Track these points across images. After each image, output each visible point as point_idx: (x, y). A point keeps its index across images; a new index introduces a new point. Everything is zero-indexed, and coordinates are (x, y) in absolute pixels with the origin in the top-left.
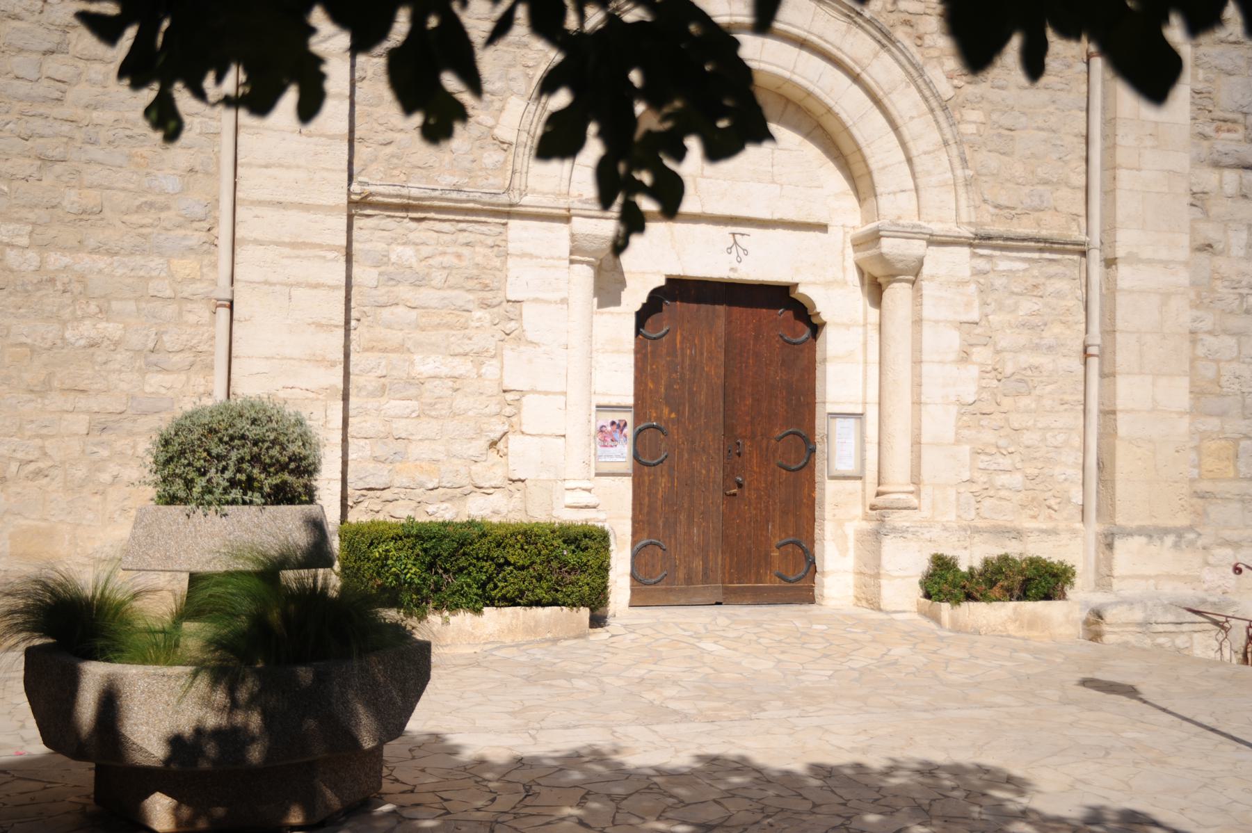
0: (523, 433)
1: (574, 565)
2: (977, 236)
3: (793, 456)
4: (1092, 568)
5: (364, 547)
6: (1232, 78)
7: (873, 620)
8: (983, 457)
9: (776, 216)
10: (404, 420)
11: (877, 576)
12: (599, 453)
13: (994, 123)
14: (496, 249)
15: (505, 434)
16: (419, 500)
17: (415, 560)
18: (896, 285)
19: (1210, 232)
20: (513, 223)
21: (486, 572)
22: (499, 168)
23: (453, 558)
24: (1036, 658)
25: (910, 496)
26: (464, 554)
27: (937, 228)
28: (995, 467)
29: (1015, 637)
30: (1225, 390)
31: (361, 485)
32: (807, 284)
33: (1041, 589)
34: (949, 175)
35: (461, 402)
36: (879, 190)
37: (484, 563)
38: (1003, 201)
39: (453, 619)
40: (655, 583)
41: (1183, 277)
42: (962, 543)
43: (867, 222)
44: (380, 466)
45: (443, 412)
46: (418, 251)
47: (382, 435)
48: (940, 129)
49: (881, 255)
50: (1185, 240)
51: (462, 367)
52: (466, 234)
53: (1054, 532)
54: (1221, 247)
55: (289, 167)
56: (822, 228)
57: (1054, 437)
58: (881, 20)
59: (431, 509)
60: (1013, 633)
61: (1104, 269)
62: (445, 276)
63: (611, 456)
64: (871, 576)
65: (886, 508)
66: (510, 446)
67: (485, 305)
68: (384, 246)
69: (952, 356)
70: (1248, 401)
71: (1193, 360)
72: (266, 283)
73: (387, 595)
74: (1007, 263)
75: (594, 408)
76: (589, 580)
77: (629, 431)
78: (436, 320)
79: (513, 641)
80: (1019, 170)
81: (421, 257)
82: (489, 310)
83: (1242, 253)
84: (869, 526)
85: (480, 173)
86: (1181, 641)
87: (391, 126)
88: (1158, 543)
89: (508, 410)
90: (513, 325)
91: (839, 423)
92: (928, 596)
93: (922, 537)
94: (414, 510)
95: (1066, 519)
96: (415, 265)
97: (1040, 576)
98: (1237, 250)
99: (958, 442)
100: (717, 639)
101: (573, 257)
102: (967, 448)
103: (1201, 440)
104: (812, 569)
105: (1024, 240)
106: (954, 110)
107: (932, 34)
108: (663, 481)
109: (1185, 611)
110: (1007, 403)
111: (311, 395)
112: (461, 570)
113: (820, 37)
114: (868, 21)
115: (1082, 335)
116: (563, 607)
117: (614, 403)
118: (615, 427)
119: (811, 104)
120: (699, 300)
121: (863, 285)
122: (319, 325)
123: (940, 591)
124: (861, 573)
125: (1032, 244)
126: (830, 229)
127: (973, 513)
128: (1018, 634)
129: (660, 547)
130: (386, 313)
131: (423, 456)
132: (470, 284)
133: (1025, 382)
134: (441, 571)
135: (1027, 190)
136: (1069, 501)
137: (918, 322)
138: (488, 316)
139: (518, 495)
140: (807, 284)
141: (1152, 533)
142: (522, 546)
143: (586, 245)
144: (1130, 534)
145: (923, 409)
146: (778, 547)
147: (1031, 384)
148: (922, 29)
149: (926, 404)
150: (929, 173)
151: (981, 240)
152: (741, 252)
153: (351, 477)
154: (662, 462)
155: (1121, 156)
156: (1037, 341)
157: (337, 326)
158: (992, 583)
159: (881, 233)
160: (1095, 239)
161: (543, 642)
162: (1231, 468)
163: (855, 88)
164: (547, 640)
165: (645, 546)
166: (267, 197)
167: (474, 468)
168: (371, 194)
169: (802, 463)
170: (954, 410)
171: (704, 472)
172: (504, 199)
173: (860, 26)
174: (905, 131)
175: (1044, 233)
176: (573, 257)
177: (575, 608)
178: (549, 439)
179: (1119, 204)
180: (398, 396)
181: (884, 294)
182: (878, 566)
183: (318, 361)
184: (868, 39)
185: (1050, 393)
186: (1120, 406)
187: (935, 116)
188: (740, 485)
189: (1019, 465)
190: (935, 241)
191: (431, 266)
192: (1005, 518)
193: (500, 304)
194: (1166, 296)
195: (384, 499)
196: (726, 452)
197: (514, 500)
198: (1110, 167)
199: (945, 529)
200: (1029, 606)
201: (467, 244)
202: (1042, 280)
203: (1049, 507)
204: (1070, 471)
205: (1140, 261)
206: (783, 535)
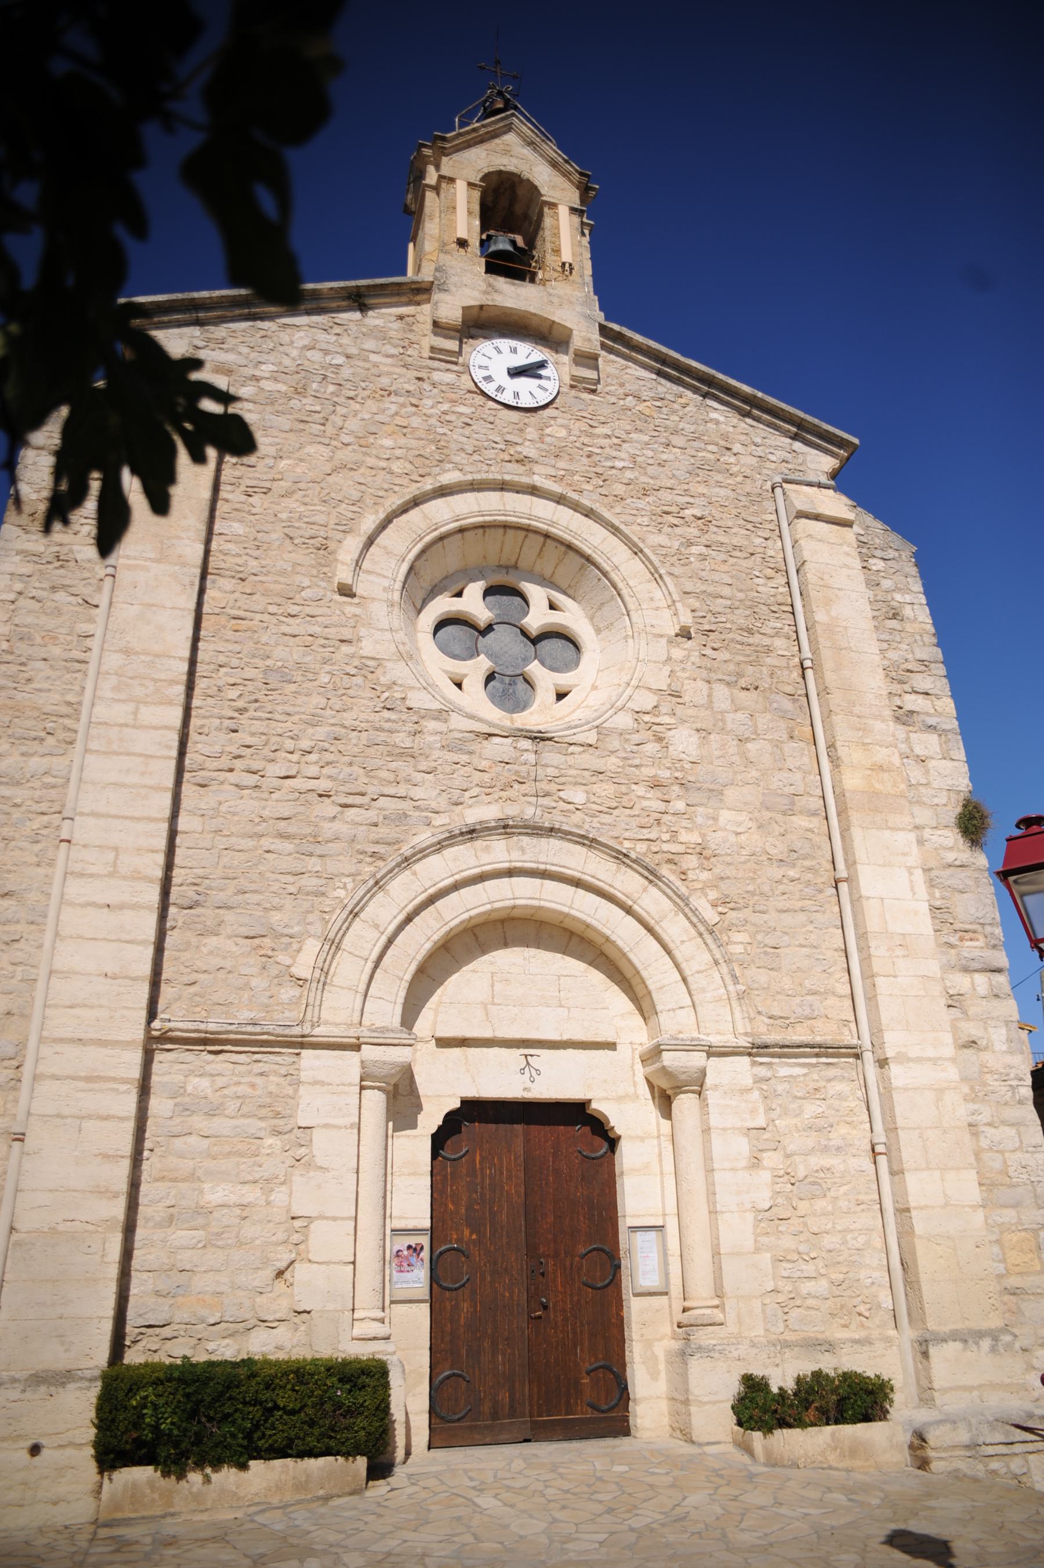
0: (310, 1261)
1: (349, 1407)
2: (754, 1046)
3: (598, 1274)
4: (912, 1380)
5: (121, 1395)
7: (682, 1455)
8: (785, 1265)
9: (565, 1037)
10: (189, 1252)
11: (686, 1402)
12: (395, 1279)
13: (760, 943)
14: (289, 1077)
15: (292, 1262)
16: (200, 1336)
17: (177, 1407)
18: (682, 1096)
19: (971, 1029)
20: (305, 1053)
21: (252, 1419)
22: (294, 1002)
23: (218, 1404)
24: (850, 1500)
25: (715, 1311)
26: (231, 1398)
27: (715, 1040)
28: (799, 1274)
29: (837, 1469)
30: (1014, 1180)
31: (141, 1322)
32: (599, 1100)
33: (858, 1410)
34: (723, 991)
35: (249, 1231)
36: (659, 1008)
37: (251, 1409)
38: (776, 1012)
39: (215, 1477)
40: (459, 1420)
41: (952, 1073)
42: (772, 1360)
43: (653, 1039)
44: (161, 1300)
45: (230, 1241)
46: (213, 1082)
47: (166, 1267)
48: (710, 950)
49: (664, 1067)
50: (948, 1038)
51: (251, 1194)
52: (260, 1064)
53: (866, 1342)
54: (985, 1043)
55: (92, 1007)
56: (611, 1046)
57: (855, 1239)
58: (647, 860)
59: (211, 1346)
60: (834, 1464)
61: (878, 1069)
62: (238, 1105)
63: (408, 1282)
64: (682, 1402)
65: (691, 1325)
66: (296, 1275)
67: (277, 1133)
68: (182, 1078)
69: (743, 1163)
70: (1039, 1190)
71: (977, 1155)
72: (59, 1116)
73: (144, 1451)
74: (786, 1069)
75: (388, 1232)
76: (365, 1423)
77: (425, 1254)
78: (227, 1148)
79: (281, 1501)
80: (787, 983)
81: (216, 1087)
82: (281, 1136)
83: (1004, 1048)
84: (676, 1345)
85: (276, 1008)
86: (1016, 1465)
87: (195, 968)
88: (975, 1348)
89: (296, 1238)
90: (303, 1151)
91: (640, 1236)
92: (740, 1424)
93: (730, 1355)
94: (194, 1347)
95: (878, 1326)
96: (210, 1095)
97: (855, 1395)
98: (1000, 1045)
99: (757, 1250)
100: (498, 1491)
101: (364, 1083)
102: (769, 1255)
103: (1002, 1233)
104: (625, 1396)
105: (799, 1047)
106: (721, 934)
107: (694, 869)
108: (465, 1306)
109: (1013, 1429)
110: (803, 1207)
111: (90, 1227)
112: (226, 1416)
113: (593, 877)
114: (634, 861)
115: (869, 1134)
116: (339, 1457)
117: (410, 1227)
118: (411, 1251)
119: (590, 934)
120: (496, 1121)
121: (653, 1098)
122: (105, 1156)
123: (751, 1418)
124: (673, 1399)
125: (808, 1050)
126: (618, 1047)
127: (781, 1325)
128: (840, 1465)
129: (464, 1379)
130: (178, 1143)
131: (207, 1289)
132: (263, 1112)
133: (819, 1184)
134: (204, 1419)
135: (798, 1000)
136: (879, 1306)
137: (706, 1130)
138: (279, 1143)
139: (303, 1328)
140: (599, 1100)
141: (967, 1337)
142: (293, 1386)
143: (376, 1071)
144: (944, 1340)
145: (719, 1217)
146: (588, 1373)
147: (824, 1186)
148: (685, 866)
149: (722, 1212)
150: (703, 990)
151: (758, 1050)
152: (533, 1072)
153: (130, 1314)
154: (463, 1285)
155: (877, 966)
156: (826, 1143)
157: (123, 1157)
158: (806, 1404)
159: (662, 1047)
160: (866, 1043)
161: (313, 1501)
162: (1037, 1261)
163: (629, 918)
164: (319, 1498)
165: (448, 1377)
166: (69, 1035)
167: (259, 1300)
168: (170, 1030)
169: (608, 1281)
170: (750, 1217)
171: (507, 1294)
172: (297, 1031)
173: (628, 866)
174: (677, 953)
175: (818, 1039)
176: (364, 1083)
177: (351, 1458)
178: (337, 1266)
179: (881, 1009)
180: (185, 1226)
181: (673, 1105)
182: (687, 1391)
183: (105, 1193)
184: (637, 875)
185: (845, 1194)
186: (912, 1204)
187: (703, 939)
188: (545, 1307)
189: (823, 1271)
190: (713, 1052)
191: (225, 1096)
192: (815, 1329)
193: (291, 1131)
194: (940, 1092)
195: (164, 1337)
196: (529, 1272)
197: (299, 1333)
198: (869, 976)
199: (753, 1345)
200: (847, 1430)
201: (262, 1074)
202: (822, 1084)
203: (860, 1315)
204: (876, 1274)
205: (910, 1060)
206: (593, 1360)
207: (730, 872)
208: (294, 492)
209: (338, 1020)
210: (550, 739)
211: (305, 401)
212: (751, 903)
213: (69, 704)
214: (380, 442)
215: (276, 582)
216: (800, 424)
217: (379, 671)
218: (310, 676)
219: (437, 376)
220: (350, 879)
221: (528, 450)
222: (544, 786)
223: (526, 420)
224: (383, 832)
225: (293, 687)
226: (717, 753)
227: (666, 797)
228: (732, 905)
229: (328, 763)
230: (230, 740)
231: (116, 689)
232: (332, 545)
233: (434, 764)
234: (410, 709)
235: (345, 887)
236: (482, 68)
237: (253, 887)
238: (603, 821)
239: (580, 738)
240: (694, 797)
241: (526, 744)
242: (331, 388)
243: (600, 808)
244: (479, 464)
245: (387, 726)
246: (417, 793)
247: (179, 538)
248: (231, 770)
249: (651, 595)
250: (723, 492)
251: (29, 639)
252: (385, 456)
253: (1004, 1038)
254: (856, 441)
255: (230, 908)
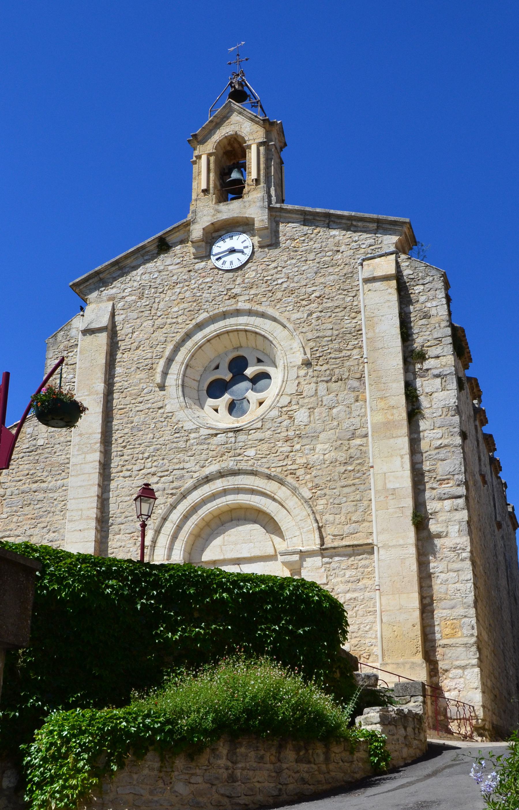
6: (445, 462)
83: (457, 535)
207: (320, 473)
208: (140, 346)
209: (159, 559)
210: (242, 430)
211: (143, 301)
212: (328, 486)
213: (67, 458)
214: (173, 310)
215: (134, 389)
216: (378, 221)
217: (173, 418)
218: (147, 426)
219: (197, 266)
220: (163, 505)
221: (237, 290)
222: (238, 451)
223: (237, 274)
224: (175, 484)
225: (141, 433)
226: (317, 418)
227: (292, 445)
228: (320, 488)
229: (155, 461)
230: (121, 459)
231: (78, 450)
232: (154, 366)
233: (194, 452)
234: (185, 431)
235: (161, 509)
236: (230, 64)
237: (130, 514)
238: (263, 461)
239: (254, 426)
240: (305, 441)
241: (231, 434)
242: (153, 290)
243: (262, 456)
244: (215, 306)
245: (175, 440)
246: (187, 466)
247: (95, 383)
248: (122, 472)
249: (291, 347)
250: (332, 278)
251: (54, 437)
252: (175, 316)
253: (457, 530)
254: (407, 220)
255: (122, 524)
